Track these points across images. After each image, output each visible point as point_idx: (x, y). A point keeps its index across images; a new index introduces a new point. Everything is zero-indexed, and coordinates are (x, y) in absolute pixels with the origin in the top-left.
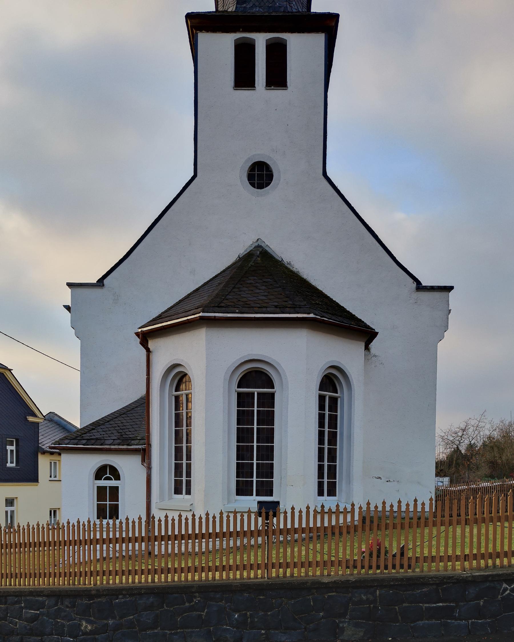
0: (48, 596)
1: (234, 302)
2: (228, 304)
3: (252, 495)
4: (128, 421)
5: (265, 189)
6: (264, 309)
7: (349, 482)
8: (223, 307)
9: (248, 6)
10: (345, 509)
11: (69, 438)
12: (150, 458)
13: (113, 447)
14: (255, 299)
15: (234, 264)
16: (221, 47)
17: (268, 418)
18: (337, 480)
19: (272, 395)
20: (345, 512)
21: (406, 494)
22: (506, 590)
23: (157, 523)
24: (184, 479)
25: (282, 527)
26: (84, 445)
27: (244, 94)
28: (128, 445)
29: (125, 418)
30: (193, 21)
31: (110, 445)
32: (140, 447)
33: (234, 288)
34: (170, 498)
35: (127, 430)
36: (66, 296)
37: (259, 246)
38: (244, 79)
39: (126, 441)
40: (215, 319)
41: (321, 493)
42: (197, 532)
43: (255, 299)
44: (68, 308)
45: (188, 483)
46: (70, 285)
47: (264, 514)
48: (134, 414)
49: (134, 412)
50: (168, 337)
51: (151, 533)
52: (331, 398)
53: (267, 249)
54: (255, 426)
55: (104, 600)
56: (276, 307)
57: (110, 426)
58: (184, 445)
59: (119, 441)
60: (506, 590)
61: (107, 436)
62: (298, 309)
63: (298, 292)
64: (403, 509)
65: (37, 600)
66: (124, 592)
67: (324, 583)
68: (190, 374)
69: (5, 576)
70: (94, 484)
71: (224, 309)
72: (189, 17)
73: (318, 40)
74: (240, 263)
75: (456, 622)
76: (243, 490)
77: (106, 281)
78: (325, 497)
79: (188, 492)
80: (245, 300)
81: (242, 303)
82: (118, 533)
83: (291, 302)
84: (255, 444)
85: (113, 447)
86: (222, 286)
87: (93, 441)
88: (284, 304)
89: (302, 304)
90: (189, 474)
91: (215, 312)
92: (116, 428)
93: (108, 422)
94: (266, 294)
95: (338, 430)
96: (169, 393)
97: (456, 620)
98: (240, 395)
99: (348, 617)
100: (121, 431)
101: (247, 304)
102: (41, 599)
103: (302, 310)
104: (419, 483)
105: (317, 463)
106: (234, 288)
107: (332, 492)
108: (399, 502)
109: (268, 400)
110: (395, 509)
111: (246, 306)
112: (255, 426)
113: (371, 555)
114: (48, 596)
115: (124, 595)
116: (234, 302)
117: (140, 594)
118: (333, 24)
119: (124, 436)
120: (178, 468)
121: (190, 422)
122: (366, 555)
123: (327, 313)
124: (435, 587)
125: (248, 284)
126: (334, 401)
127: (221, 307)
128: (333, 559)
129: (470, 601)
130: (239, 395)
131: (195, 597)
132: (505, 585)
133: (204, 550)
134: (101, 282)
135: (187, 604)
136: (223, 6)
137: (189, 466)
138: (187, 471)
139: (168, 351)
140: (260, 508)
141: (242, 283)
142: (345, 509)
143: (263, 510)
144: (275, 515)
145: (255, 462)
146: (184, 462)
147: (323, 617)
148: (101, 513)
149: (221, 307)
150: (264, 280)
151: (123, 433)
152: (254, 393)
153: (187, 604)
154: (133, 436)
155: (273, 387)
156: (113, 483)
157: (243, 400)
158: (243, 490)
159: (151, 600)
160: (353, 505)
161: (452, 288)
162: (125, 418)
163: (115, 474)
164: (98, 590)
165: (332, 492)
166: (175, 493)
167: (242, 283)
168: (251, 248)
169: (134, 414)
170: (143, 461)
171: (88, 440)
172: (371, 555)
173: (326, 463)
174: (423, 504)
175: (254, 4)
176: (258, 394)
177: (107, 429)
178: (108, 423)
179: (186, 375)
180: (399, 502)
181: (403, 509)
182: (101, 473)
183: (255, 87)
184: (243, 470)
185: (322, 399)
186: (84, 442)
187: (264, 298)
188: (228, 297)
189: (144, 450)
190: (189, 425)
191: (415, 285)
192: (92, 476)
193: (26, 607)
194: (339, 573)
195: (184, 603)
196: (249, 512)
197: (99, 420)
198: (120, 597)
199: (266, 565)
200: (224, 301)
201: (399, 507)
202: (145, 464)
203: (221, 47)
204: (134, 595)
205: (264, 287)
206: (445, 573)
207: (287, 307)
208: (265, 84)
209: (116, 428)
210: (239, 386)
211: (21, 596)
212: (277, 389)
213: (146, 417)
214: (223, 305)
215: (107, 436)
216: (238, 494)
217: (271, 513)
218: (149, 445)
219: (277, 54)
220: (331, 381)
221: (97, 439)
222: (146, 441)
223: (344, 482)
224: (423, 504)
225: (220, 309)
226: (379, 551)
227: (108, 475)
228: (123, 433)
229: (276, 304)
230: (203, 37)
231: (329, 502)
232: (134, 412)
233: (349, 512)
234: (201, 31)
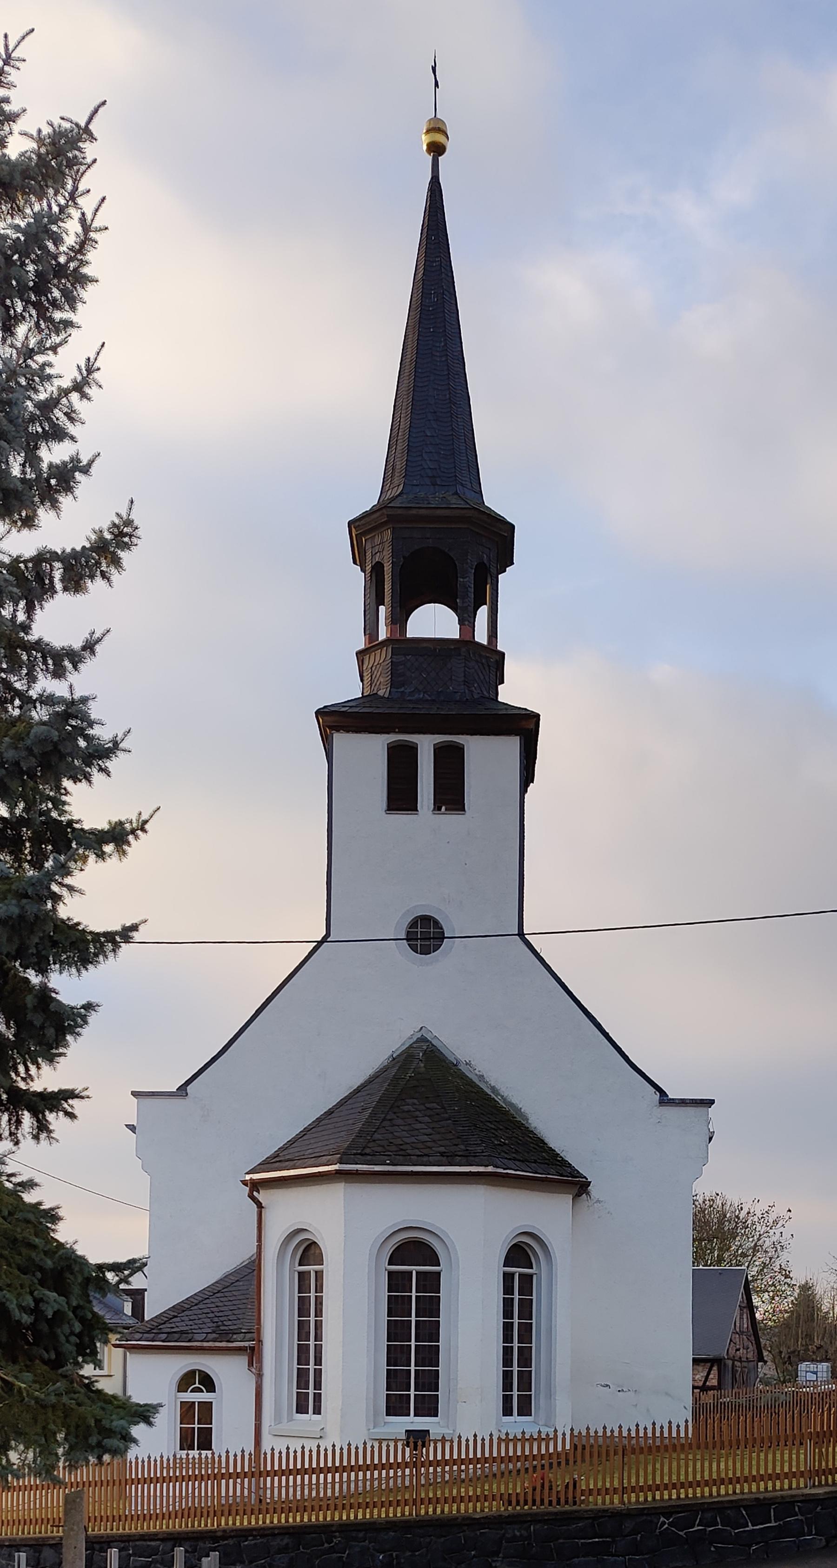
0: (163, 1540)
1: (383, 1146)
2: (376, 1149)
3: (409, 1415)
4: (226, 1304)
5: (433, 954)
6: (425, 1159)
7: (550, 1395)
8: (368, 1155)
9: (408, 691)
10: (547, 1435)
11: (140, 1331)
12: (260, 1361)
13: (205, 1344)
14: (413, 1139)
15: (384, 1070)
16: (369, 753)
17: (431, 1307)
18: (533, 1393)
19: (438, 1274)
20: (547, 1439)
22: (664, 1523)
23: (262, 1456)
24: (311, 1391)
25: (431, 1458)
26: (163, 1341)
27: (401, 819)
28: (228, 1341)
29: (222, 1299)
30: (325, 718)
31: (201, 1341)
32: (246, 1344)
33: (384, 1119)
34: (290, 1419)
35: (225, 1318)
36: (130, 1110)
37: (423, 1039)
38: (401, 798)
39: (226, 1335)
40: (357, 1173)
41: (507, 1411)
42: (337, 1464)
43: (413, 1139)
44: (132, 1128)
45: (318, 1398)
46: (135, 1094)
47: (412, 1444)
48: (234, 1293)
49: (234, 1288)
50: (290, 1189)
51: (257, 1469)
52: (521, 1275)
53: (434, 1042)
54: (413, 1319)
55: (231, 1542)
56: (442, 1154)
57: (200, 1312)
59: (214, 1335)
60: (664, 1523)
61: (196, 1327)
62: (472, 1158)
63: (475, 1125)
64: (625, 1434)
65: (148, 1546)
66: (254, 1533)
67: (475, 1519)
69: (105, 1519)
70: (176, 1398)
71: (369, 1158)
72: (320, 713)
73: (512, 745)
74: (394, 1070)
75: (612, 1559)
76: (396, 1406)
77: (189, 1088)
78: (515, 1417)
79: (317, 1411)
80: (399, 1141)
81: (394, 1148)
82: (190, 1471)
83: (462, 1147)
84: (413, 1343)
85: (205, 1344)
86: (367, 1113)
87: (176, 1336)
88: (453, 1149)
89: (479, 1149)
91: (357, 1164)
92: (209, 1315)
93: (196, 1305)
94: (430, 1131)
95: (534, 1321)
96: (291, 1269)
97: (613, 1556)
99: (501, 1555)
100: (216, 1320)
101: (402, 1150)
102: (153, 1543)
103: (477, 1159)
104: (667, 1394)
105: (501, 1369)
106: (384, 1119)
107: (525, 1409)
108: (620, 1427)
109: (431, 1282)
110: (616, 1434)
111: (400, 1153)
112: (413, 1319)
113: (534, 1489)
114: (163, 1540)
115: (255, 1536)
116: (383, 1146)
117: (274, 1535)
118: (532, 726)
119: (222, 1328)
120: (302, 1375)
121: (321, 1311)
122: (530, 1491)
123: (515, 1159)
124: (590, 1521)
125: (404, 1112)
126: (527, 1282)
127: (366, 1154)
128: (486, 1493)
129: (627, 1536)
130: (391, 1274)
131: (335, 1537)
132: (662, 1519)
133: (337, 1495)
134: (183, 1090)
135: (326, 1545)
136: (371, 684)
137: (318, 1373)
139: (289, 1211)
140: (408, 1438)
141: (396, 1110)
142: (547, 1435)
143: (412, 1440)
144: (423, 1446)
145: (413, 1368)
146: (312, 1367)
147: (474, 1556)
148: (186, 1442)
149: (366, 1154)
150: (428, 1105)
151: (220, 1323)
152: (412, 1272)
153: (326, 1545)
154: (235, 1327)
156: (204, 1396)
157: (397, 1282)
158: (396, 1406)
159: (286, 1541)
160: (556, 1431)
161: (712, 1102)
162: (222, 1299)
163: (208, 1383)
164: (224, 1531)
165: (525, 1409)
166: (297, 1412)
167: (396, 1110)
168: (412, 1041)
169: (234, 1293)
170: (251, 1364)
171: (168, 1333)
172: (534, 1489)
173: (515, 1369)
174: (645, 1429)
175: (416, 688)
176: (417, 1273)
177: (195, 1317)
178: (196, 1307)
180: (620, 1427)
181: (625, 1434)
182: (186, 1382)
183: (417, 810)
184: (396, 1380)
185: (508, 1278)
186: (164, 1336)
187: (426, 1138)
188: (376, 1136)
189: (252, 1349)
190: (319, 1312)
192: (174, 1387)
193: (134, 1555)
194: (495, 1508)
195: (323, 1545)
196: (396, 1441)
197: (182, 1302)
198: (250, 1538)
199: (414, 1501)
200: (370, 1145)
201: (620, 1432)
202: (253, 1370)
203: (369, 753)
204: (266, 1535)
205: (427, 1119)
206: (603, 1507)
207: (457, 1155)
208: (432, 806)
209: (209, 1315)
211: (129, 1541)
212: (443, 1267)
213: (255, 1301)
214: (368, 1151)
215: (196, 1327)
217: (420, 1443)
218: (260, 1341)
219: (450, 764)
220: (519, 1254)
221: (182, 1332)
222: (255, 1335)
223: (542, 1396)
224: (645, 1429)
225: (363, 1158)
226: (543, 1486)
227: (197, 1385)
228: (220, 1323)
229: (442, 1149)
230: (340, 739)
231: (516, 1424)
232: (234, 1288)
233: (535, 1439)
234: (338, 731)
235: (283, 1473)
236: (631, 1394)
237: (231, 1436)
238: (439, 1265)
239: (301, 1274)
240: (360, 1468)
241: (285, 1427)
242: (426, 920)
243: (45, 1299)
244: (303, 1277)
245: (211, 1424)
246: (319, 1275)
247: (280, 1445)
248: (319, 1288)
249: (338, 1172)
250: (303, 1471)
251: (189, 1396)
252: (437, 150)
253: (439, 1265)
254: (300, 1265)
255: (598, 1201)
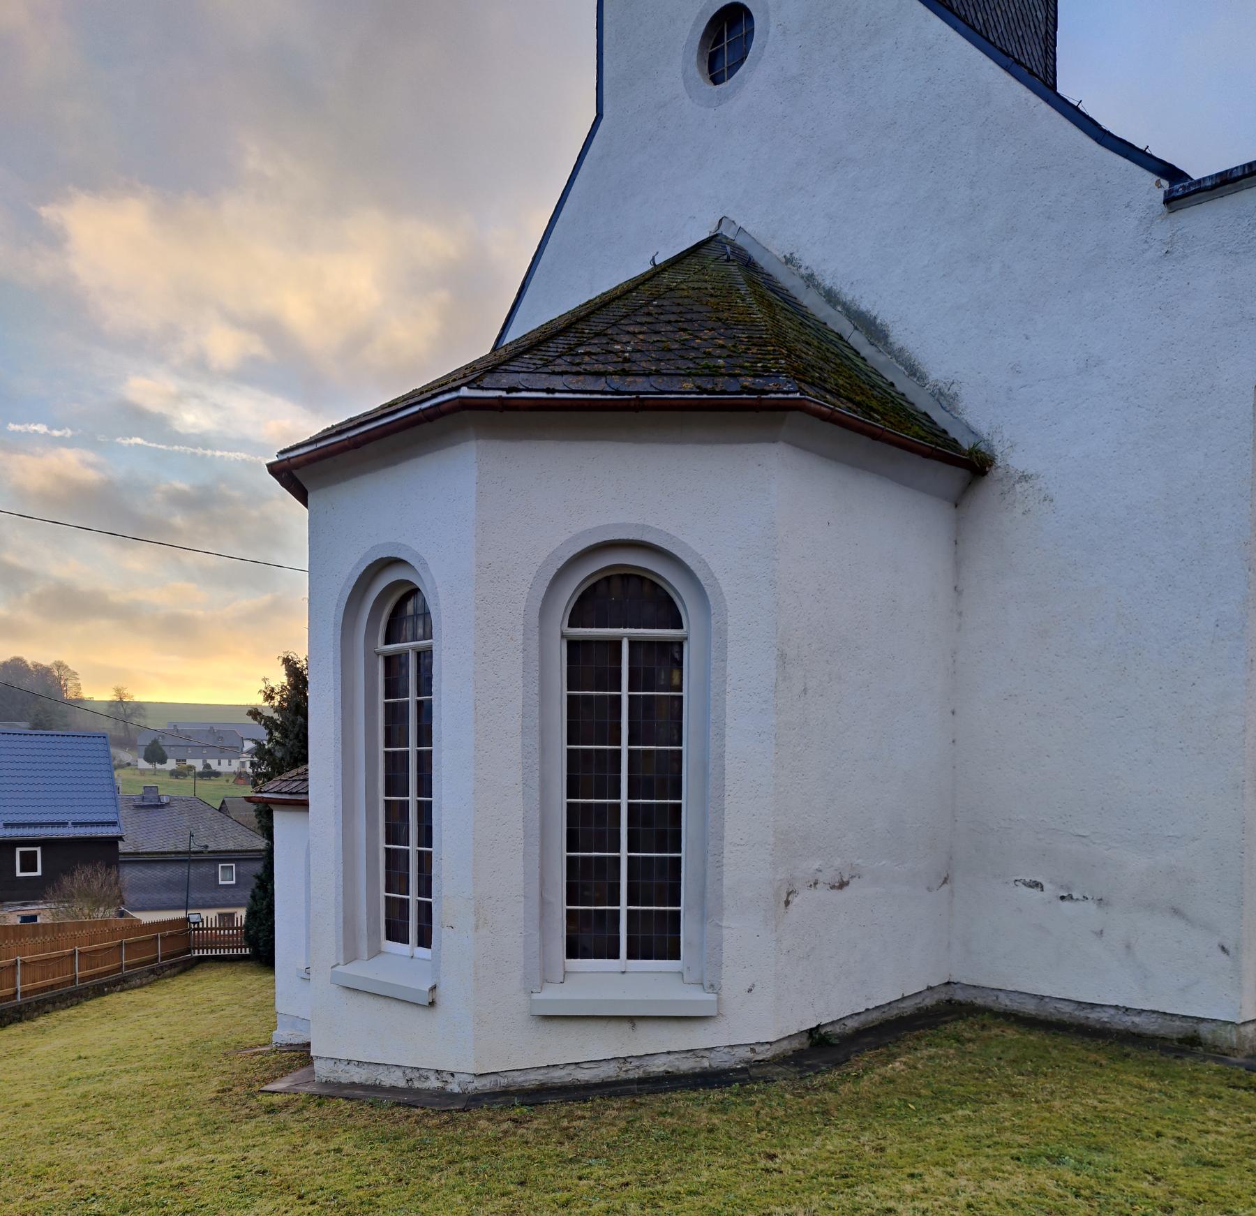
3: (617, 956)
17: (662, 720)
21: (1128, 947)
24: (413, 798)
34: (376, 952)
45: (426, 911)
58: (412, 748)
68: (426, 590)
79: (425, 940)
90: (425, 786)
98: (575, 648)
105: (433, 850)
109: (662, 662)
112: (624, 801)
138: (419, 728)
145: (624, 854)
146: (412, 698)
155: (678, 624)
157: (588, 663)
166: (389, 938)
176: (633, 644)
179: (416, 591)
184: (586, 881)
191: (1151, 188)
210: (576, 619)
216: (573, 951)
236: (1091, 906)
238: (680, 626)
239: (390, 661)
243: (1198, 1037)
244: (393, 664)
246: (425, 657)
248: (425, 684)
253: (680, 626)
254: (387, 642)
255: (1025, 478)
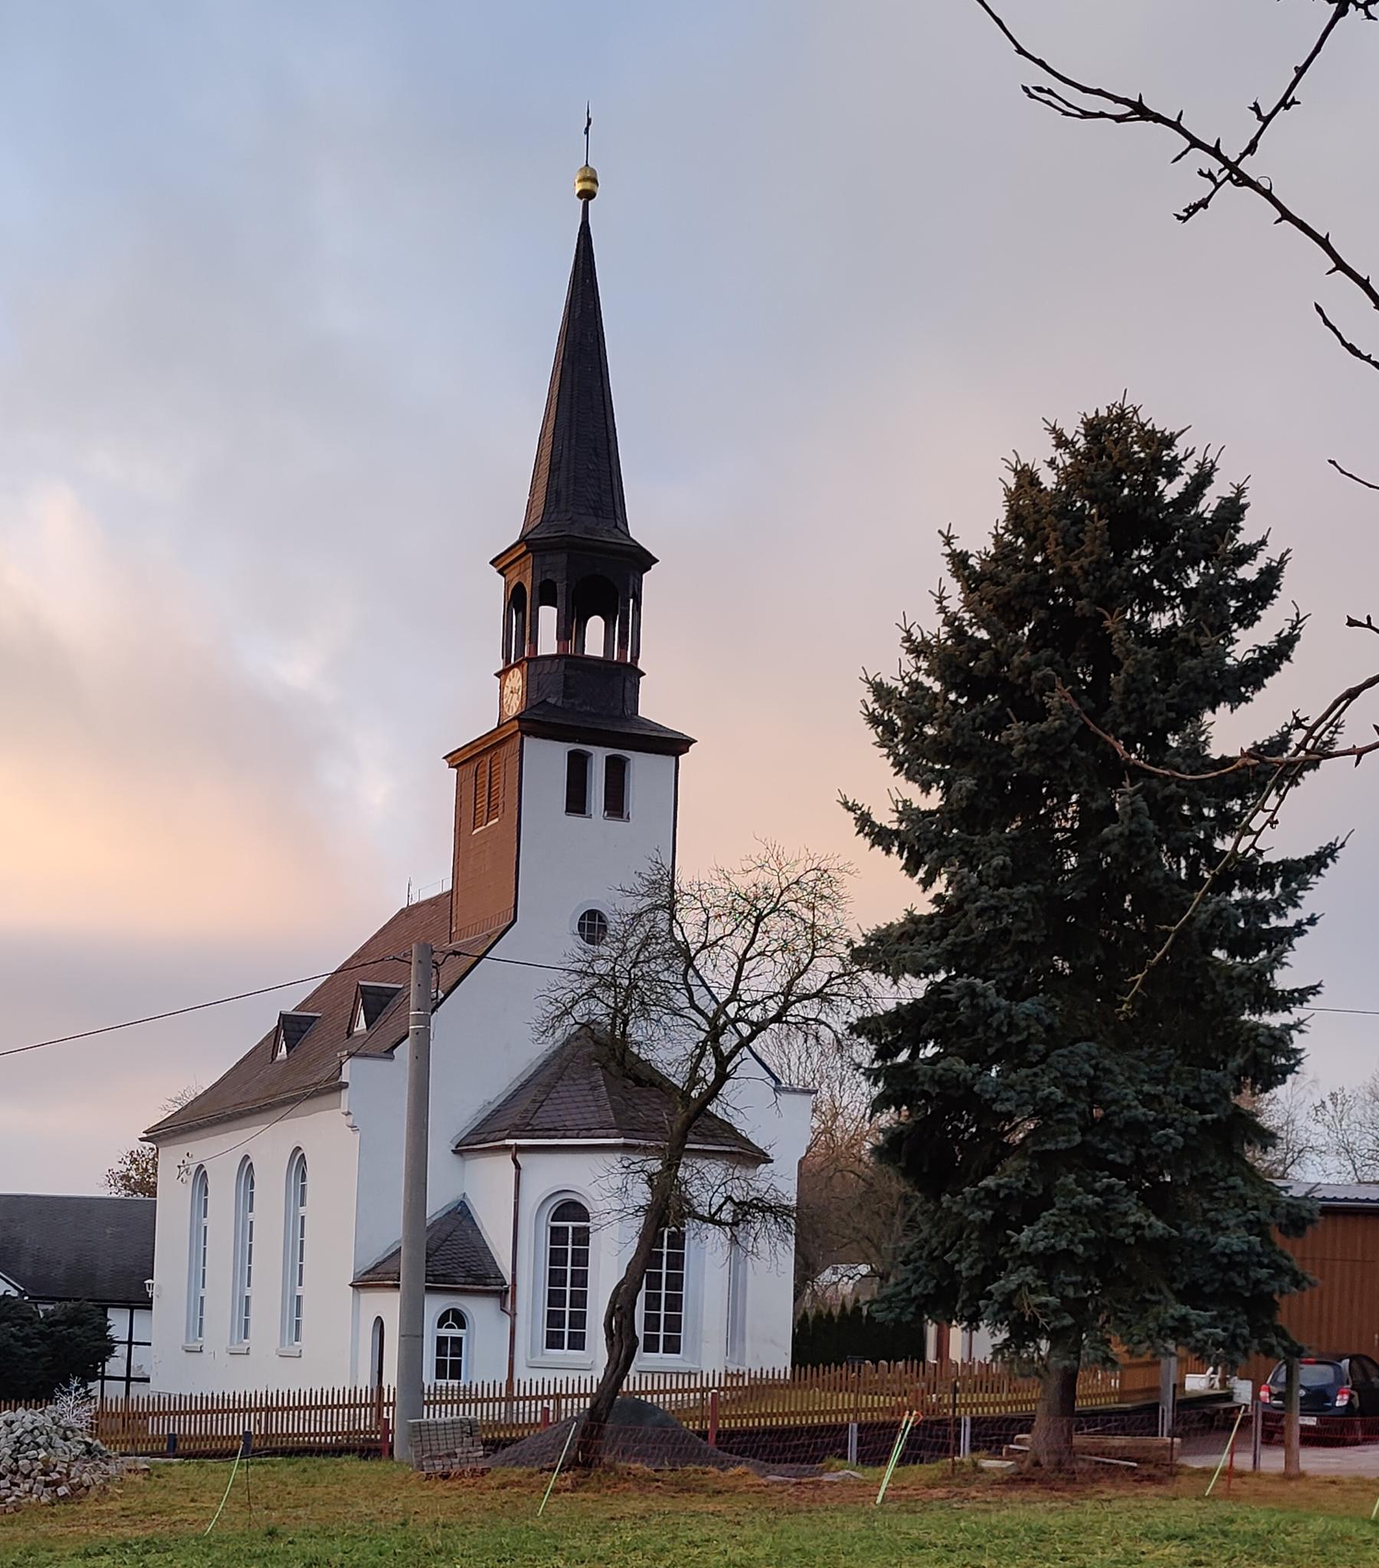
27: (576, 820)
38: (576, 803)
130: (552, 1228)
156: (456, 1332)
219: (616, 771)
235: (576, 1396)
237: (484, 1365)
240: (667, 1392)
241: (538, 1359)
242: (592, 914)
245: (664, 1352)
247: (537, 1376)
249: (625, 1146)
250: (537, 1398)
251: (445, 1332)
252: (587, 195)
